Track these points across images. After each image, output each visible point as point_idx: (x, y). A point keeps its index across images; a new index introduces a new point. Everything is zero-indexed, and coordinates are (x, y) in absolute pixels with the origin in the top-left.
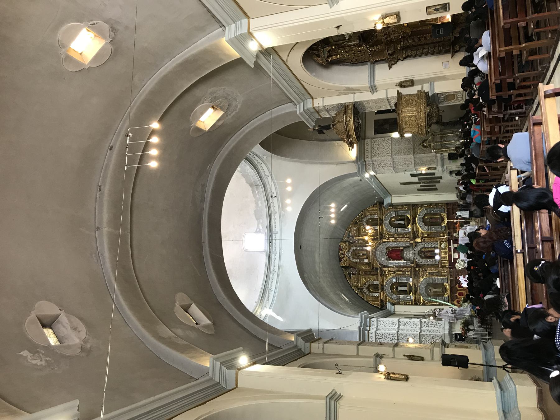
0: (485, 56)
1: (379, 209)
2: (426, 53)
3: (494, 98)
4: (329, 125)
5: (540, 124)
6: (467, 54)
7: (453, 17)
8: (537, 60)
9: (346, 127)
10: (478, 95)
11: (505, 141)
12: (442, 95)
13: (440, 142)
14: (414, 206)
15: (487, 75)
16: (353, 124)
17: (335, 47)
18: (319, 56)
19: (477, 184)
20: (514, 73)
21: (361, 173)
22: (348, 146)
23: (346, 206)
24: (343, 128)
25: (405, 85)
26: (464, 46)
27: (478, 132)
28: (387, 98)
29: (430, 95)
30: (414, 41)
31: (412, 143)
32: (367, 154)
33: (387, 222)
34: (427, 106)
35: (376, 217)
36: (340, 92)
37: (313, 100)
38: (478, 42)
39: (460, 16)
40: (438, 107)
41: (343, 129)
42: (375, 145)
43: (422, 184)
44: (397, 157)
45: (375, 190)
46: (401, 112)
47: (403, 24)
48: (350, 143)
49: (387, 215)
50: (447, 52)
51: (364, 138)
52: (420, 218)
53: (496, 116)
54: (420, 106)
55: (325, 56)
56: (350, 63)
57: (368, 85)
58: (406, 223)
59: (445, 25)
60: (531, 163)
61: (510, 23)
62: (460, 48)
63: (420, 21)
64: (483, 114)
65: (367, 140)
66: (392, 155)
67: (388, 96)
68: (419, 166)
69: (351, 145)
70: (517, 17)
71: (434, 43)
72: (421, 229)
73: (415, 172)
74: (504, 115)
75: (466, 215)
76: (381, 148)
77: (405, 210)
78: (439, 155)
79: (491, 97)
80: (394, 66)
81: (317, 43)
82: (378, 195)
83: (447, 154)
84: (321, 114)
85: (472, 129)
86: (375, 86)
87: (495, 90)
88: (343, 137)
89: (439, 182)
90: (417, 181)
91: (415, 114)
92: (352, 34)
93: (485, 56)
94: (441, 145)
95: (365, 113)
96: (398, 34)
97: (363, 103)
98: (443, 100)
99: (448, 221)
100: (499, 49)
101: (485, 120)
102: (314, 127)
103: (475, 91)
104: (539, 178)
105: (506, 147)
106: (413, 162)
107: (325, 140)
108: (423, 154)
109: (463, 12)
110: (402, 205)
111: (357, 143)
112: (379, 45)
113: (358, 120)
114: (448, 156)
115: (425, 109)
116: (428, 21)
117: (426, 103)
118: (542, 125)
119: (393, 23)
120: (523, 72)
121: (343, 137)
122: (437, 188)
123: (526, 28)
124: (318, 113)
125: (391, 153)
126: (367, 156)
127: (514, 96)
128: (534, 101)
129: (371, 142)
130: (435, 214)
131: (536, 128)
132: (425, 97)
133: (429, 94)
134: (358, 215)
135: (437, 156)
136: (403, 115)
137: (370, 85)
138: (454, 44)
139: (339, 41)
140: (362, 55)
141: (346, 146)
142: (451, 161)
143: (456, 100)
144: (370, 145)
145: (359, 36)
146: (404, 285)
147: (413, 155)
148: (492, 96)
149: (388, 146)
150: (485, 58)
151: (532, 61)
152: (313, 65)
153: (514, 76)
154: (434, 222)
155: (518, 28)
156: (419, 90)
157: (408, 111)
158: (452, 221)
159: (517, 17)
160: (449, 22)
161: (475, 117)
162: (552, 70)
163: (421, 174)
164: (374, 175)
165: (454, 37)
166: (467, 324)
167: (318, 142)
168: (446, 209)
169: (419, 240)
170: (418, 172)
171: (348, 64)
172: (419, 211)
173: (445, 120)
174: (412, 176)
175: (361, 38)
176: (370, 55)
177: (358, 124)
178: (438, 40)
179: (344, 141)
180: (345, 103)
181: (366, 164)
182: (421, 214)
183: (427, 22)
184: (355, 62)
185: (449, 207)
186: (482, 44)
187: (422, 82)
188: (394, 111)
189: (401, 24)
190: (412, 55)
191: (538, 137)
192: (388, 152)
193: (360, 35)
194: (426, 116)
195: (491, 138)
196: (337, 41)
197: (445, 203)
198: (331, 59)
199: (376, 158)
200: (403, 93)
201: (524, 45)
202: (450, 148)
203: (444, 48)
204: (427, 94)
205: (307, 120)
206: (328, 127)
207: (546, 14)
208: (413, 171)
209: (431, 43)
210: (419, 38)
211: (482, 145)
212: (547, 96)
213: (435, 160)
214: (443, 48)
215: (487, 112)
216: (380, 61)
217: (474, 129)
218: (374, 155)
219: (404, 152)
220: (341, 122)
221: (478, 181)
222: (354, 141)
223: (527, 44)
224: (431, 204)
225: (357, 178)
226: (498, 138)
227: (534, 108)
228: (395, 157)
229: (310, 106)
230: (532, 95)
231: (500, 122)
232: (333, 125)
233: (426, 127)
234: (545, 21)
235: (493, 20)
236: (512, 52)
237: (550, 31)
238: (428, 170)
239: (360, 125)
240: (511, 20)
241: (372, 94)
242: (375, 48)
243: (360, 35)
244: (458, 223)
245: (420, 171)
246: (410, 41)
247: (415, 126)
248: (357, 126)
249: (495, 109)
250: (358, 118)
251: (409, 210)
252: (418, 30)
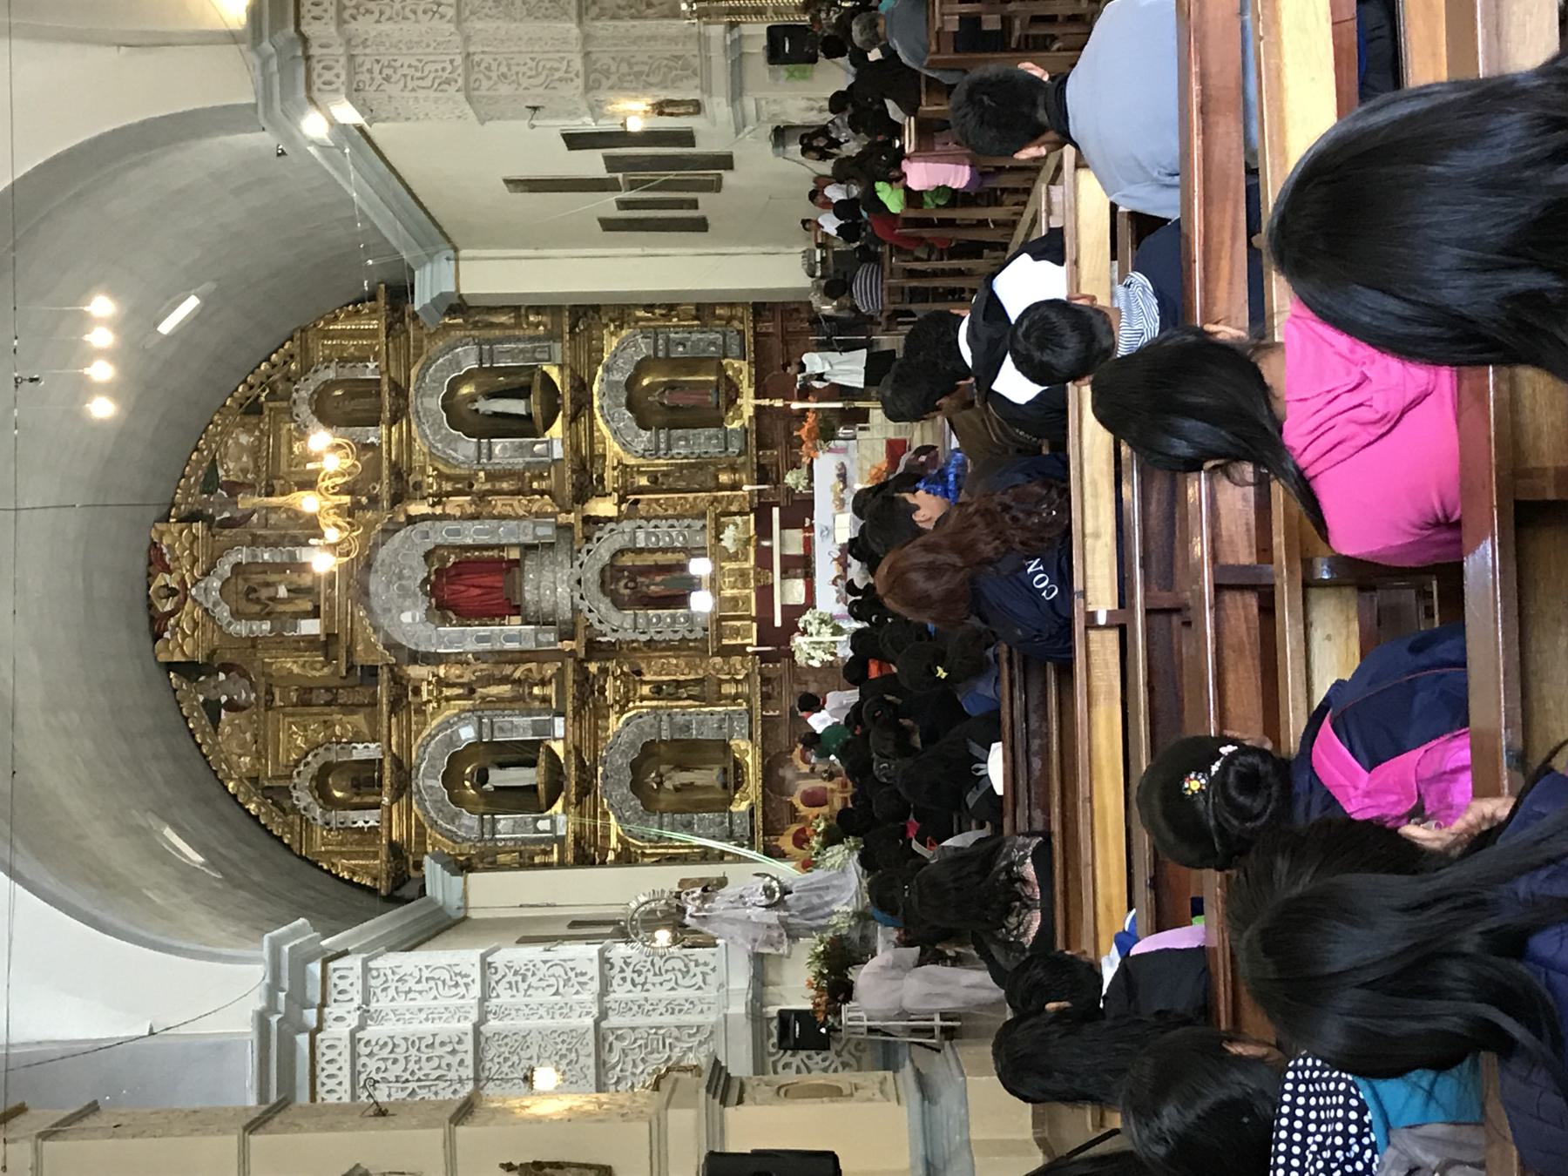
146: (524, 754)
169: (604, 507)
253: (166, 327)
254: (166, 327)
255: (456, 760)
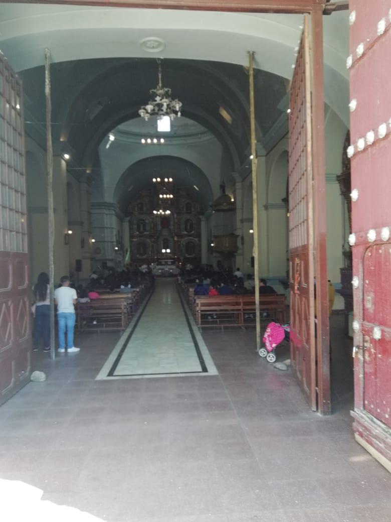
14: (199, 235)
72: (184, 241)
146: (145, 229)
166: (110, 269)
169: (176, 239)
253: (195, 186)
254: (195, 186)
255: (143, 220)
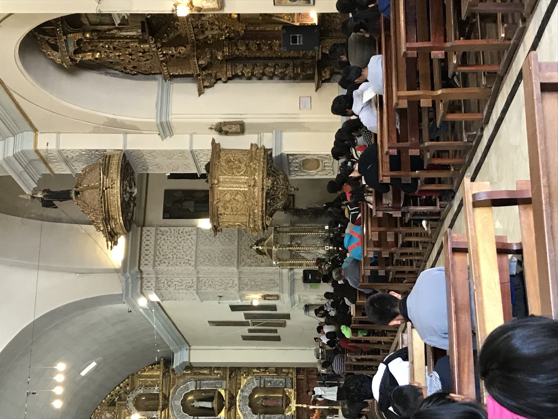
0: (373, 101)
1: (164, 374)
2: (271, 75)
3: (387, 180)
4: (68, 192)
5: (465, 251)
6: (344, 92)
7: (322, 17)
8: (461, 122)
9: (105, 201)
10: (359, 171)
11: (404, 260)
12: (297, 159)
13: (289, 246)
15: (376, 135)
16: (119, 195)
17: (91, 35)
18: (55, 48)
19: (354, 338)
20: (421, 141)
21: (130, 295)
22: (105, 239)
23: (94, 364)
24: (97, 200)
25: (228, 130)
26: (338, 73)
27: (357, 240)
28: (192, 152)
29: (274, 155)
30: (248, 49)
31: (236, 244)
32: (147, 257)
33: (178, 403)
34: (267, 177)
35: (156, 390)
36: (96, 127)
37: (36, 136)
38: (360, 75)
39: (333, 17)
40: (288, 181)
41: (96, 202)
42: (164, 240)
43: (251, 327)
44: (206, 268)
45: (158, 334)
46: (216, 182)
47: (231, 14)
48: (110, 233)
49: (178, 387)
50: (309, 78)
51: (142, 224)
52: (244, 397)
53: (390, 213)
54: (254, 175)
55: (68, 51)
56: (122, 71)
57: (155, 120)
58: (215, 406)
59: (306, 29)
60: (449, 333)
61: (418, 49)
62: (331, 75)
63: (261, 15)
64: (367, 206)
65: (148, 228)
66: (196, 264)
67: (194, 148)
68: (248, 290)
69: (112, 237)
70: (429, 40)
71: (286, 58)
73: (238, 302)
74: (404, 214)
75: (332, 395)
76: (175, 248)
77: (215, 379)
78: (285, 271)
79: (381, 179)
80: (207, 91)
81: (53, 22)
82: (161, 343)
83: (301, 271)
84: (51, 165)
85: (347, 231)
86: (168, 123)
87: (388, 166)
88: (97, 218)
89: (283, 325)
90: (243, 319)
91: (243, 189)
92: (128, 16)
93: (373, 101)
94: (291, 253)
95: (148, 174)
96: (219, 31)
97: (143, 156)
98: (297, 167)
99: (297, 408)
100: (396, 94)
101: (369, 218)
102: (35, 191)
103: (353, 163)
104: (462, 360)
105: (404, 301)
106: (236, 282)
107: (58, 220)
108: (256, 266)
109: (337, 11)
110: (210, 368)
111: (126, 234)
112: (182, 46)
113: (131, 187)
114: (302, 275)
115: (263, 181)
116: (277, 17)
117: (265, 171)
118: (467, 253)
119: (210, 10)
120: (438, 140)
121: (97, 218)
122: (279, 337)
123: (445, 61)
124: (46, 163)
125: (194, 259)
126: (146, 262)
127: (421, 181)
128: (455, 193)
129: (157, 234)
130: (274, 390)
131: (458, 258)
132: (264, 158)
133: (271, 154)
134: (119, 385)
135: (282, 274)
136: (220, 188)
137: (159, 122)
138: (321, 64)
139: (101, 24)
140: (147, 60)
141: (102, 239)
142: (308, 285)
143: (322, 171)
144: (153, 238)
145: (143, 23)
147: (238, 268)
148: (383, 176)
149: (190, 245)
150: (373, 104)
151: (453, 123)
152: (40, 62)
153: (422, 146)
154: (270, 407)
155: (431, 60)
156: (253, 143)
157: (230, 182)
158: (305, 406)
159: (429, 40)
160: (313, 26)
161: (355, 210)
162: (485, 144)
163: (250, 307)
164: (159, 303)
165: (322, 53)
167: (40, 222)
168: (295, 380)
170: (245, 303)
171: (117, 72)
172: (244, 382)
173: (300, 204)
174: (234, 308)
175: (146, 25)
176: (162, 61)
177: (131, 196)
178: (292, 54)
179: (98, 229)
180: (105, 151)
181: (142, 278)
182: (247, 389)
183: (274, 18)
184: (131, 71)
185: (300, 377)
186: (368, 79)
187: (260, 128)
188: (203, 176)
189: (226, 14)
190: (243, 75)
191: (460, 277)
192: (188, 258)
193: (144, 20)
194: (265, 195)
195: (380, 253)
196: (97, 25)
197: (293, 368)
198: (82, 58)
199: (162, 267)
200: (223, 146)
201: (439, 92)
202: (307, 260)
203: (303, 71)
204: (267, 153)
205: (19, 175)
206: (65, 196)
207: (480, 42)
208: (235, 299)
209: (281, 58)
210: (258, 45)
211: (364, 265)
212: (477, 204)
213: (278, 282)
214: (303, 71)
215: (374, 204)
216: (179, 76)
217: (351, 231)
218: (160, 261)
219: (221, 259)
220: (93, 188)
221: (354, 331)
222: (118, 230)
223: (445, 91)
224: (266, 368)
225: (123, 307)
226: (392, 254)
227: (455, 208)
228: (203, 268)
229: (29, 147)
230: (452, 183)
231: (396, 226)
232: (77, 193)
233: (262, 217)
234: (477, 54)
235: (388, 37)
236: (419, 101)
237: (484, 73)
238: (265, 299)
239: (135, 198)
240: (420, 45)
241: (163, 140)
242: (172, 51)
243: (144, 20)
244: (317, 412)
245: (248, 300)
246: (243, 48)
247: (242, 212)
248: (127, 199)
249: (388, 200)
250: (130, 183)
251: (223, 378)
252: (257, 29)
